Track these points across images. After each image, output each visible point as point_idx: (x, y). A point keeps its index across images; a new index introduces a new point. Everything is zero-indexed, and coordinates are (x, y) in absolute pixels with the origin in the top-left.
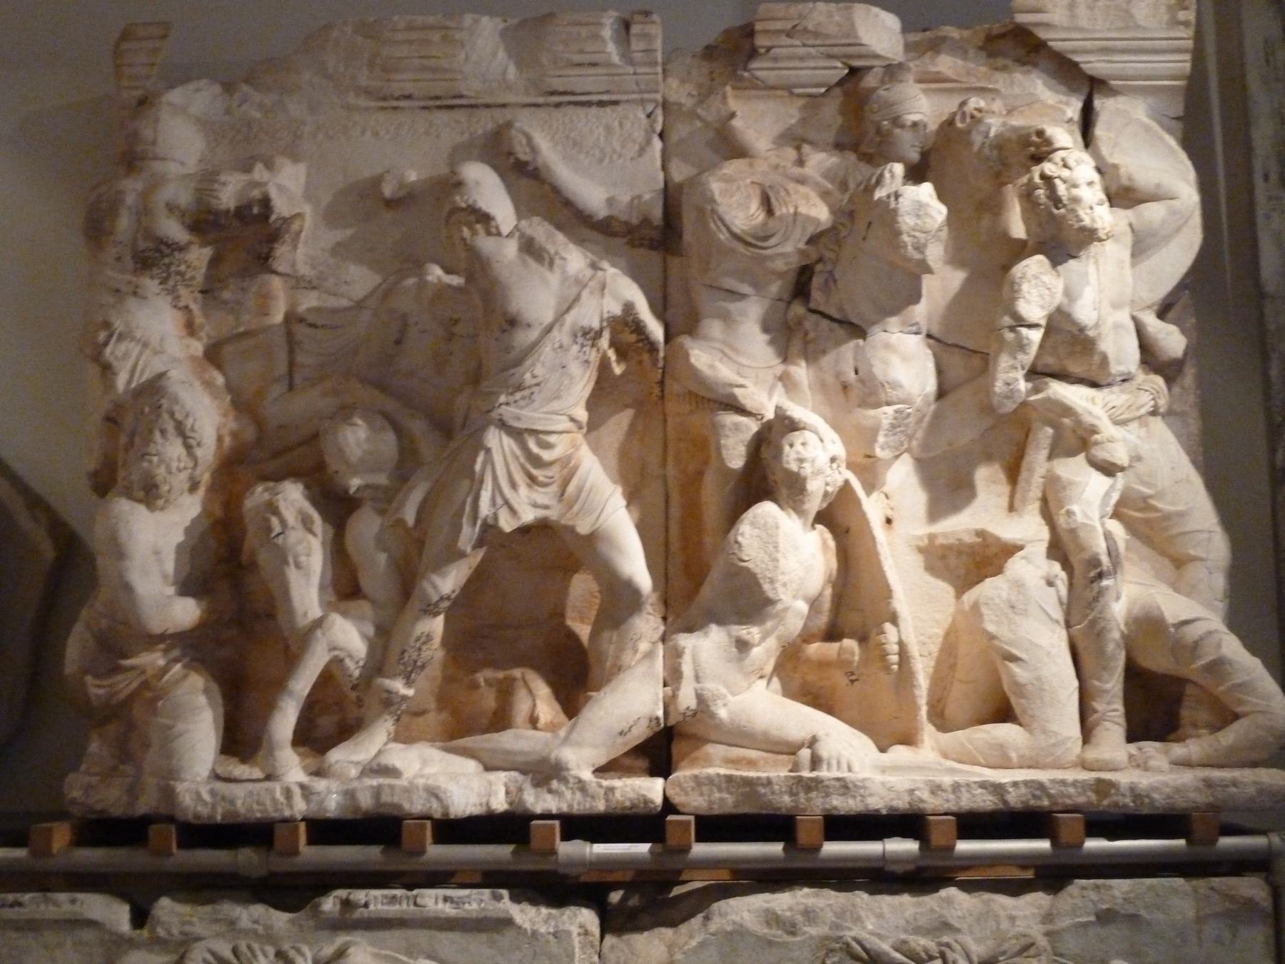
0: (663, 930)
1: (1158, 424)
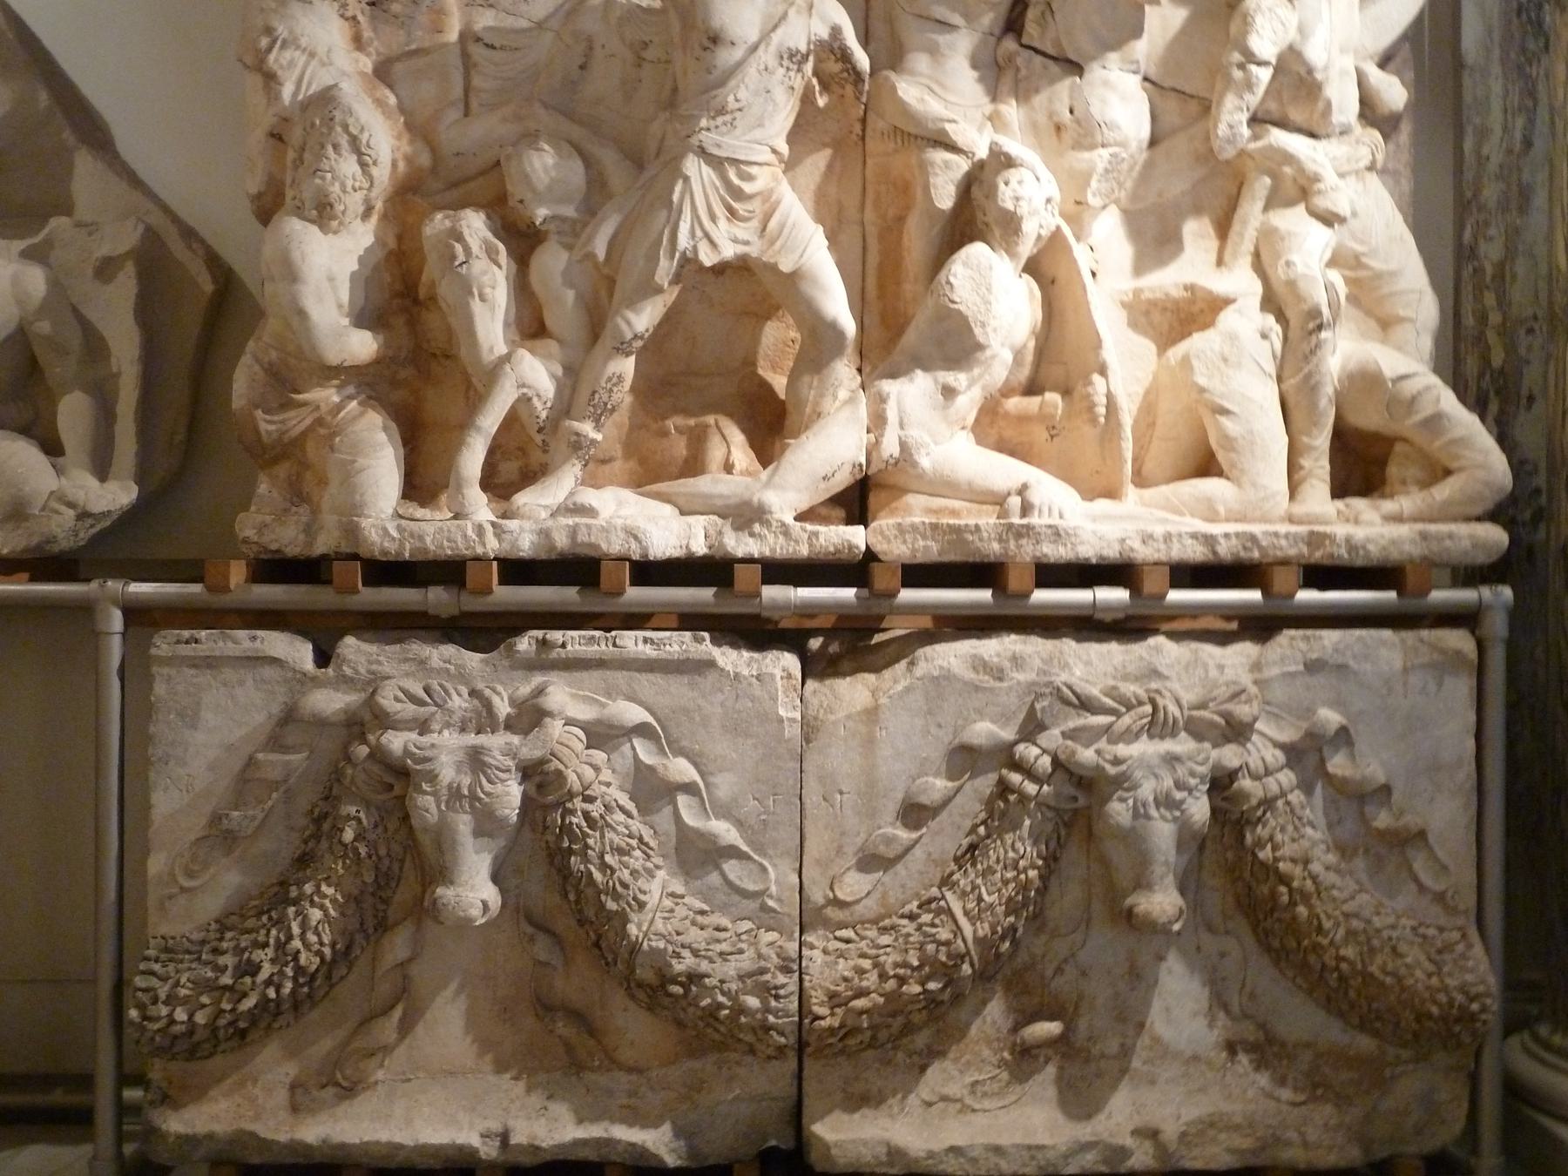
0: (866, 675)
1: (1373, 180)
